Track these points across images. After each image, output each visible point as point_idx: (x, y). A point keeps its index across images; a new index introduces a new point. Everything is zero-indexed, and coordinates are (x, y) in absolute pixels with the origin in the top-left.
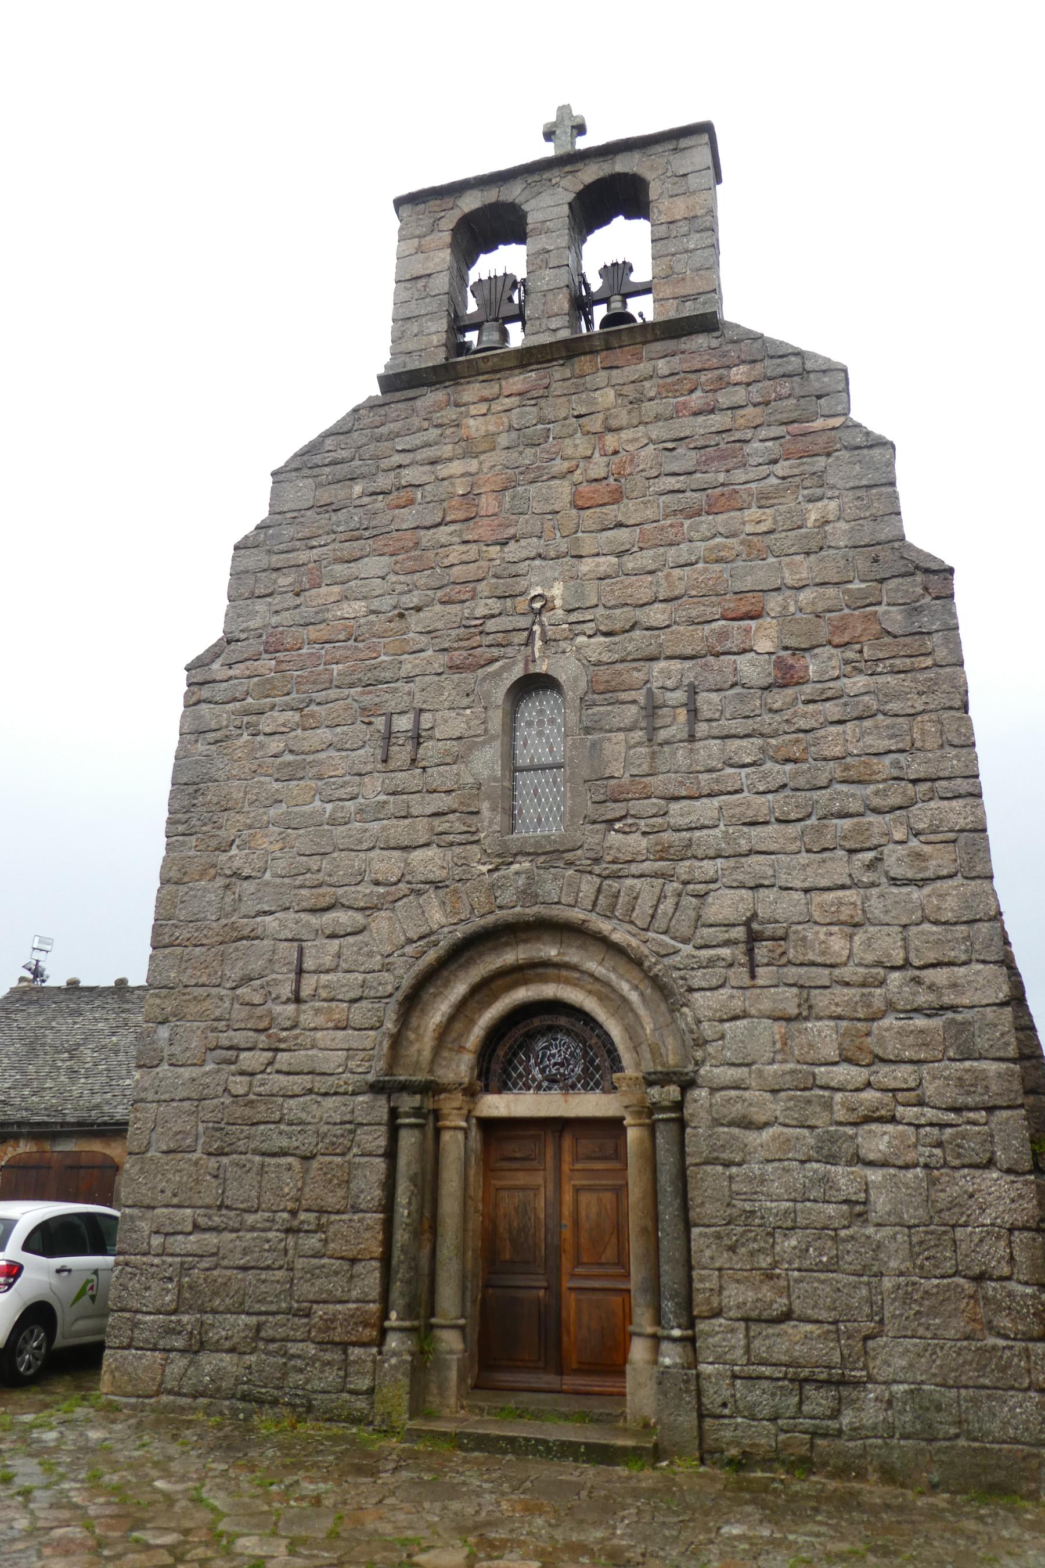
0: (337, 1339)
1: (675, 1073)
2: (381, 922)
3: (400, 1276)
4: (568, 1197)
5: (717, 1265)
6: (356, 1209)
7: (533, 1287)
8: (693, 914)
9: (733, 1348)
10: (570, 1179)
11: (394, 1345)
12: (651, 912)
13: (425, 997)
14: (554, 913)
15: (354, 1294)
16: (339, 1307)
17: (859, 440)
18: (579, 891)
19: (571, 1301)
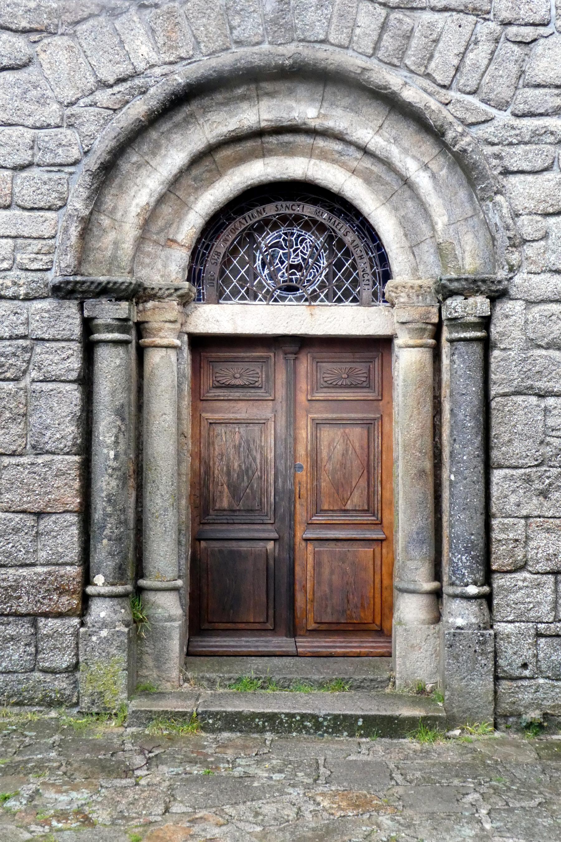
0: (23, 610)
1: (484, 281)
2: (55, 54)
3: (107, 532)
4: (304, 433)
5: (524, 513)
6: (38, 450)
7: (258, 541)
8: (514, 69)
9: (539, 603)
10: (308, 412)
11: (103, 614)
12: (456, 62)
13: (125, 166)
14: (321, 55)
15: (43, 555)
16: (24, 572)
18: (355, 25)
19: (306, 555)
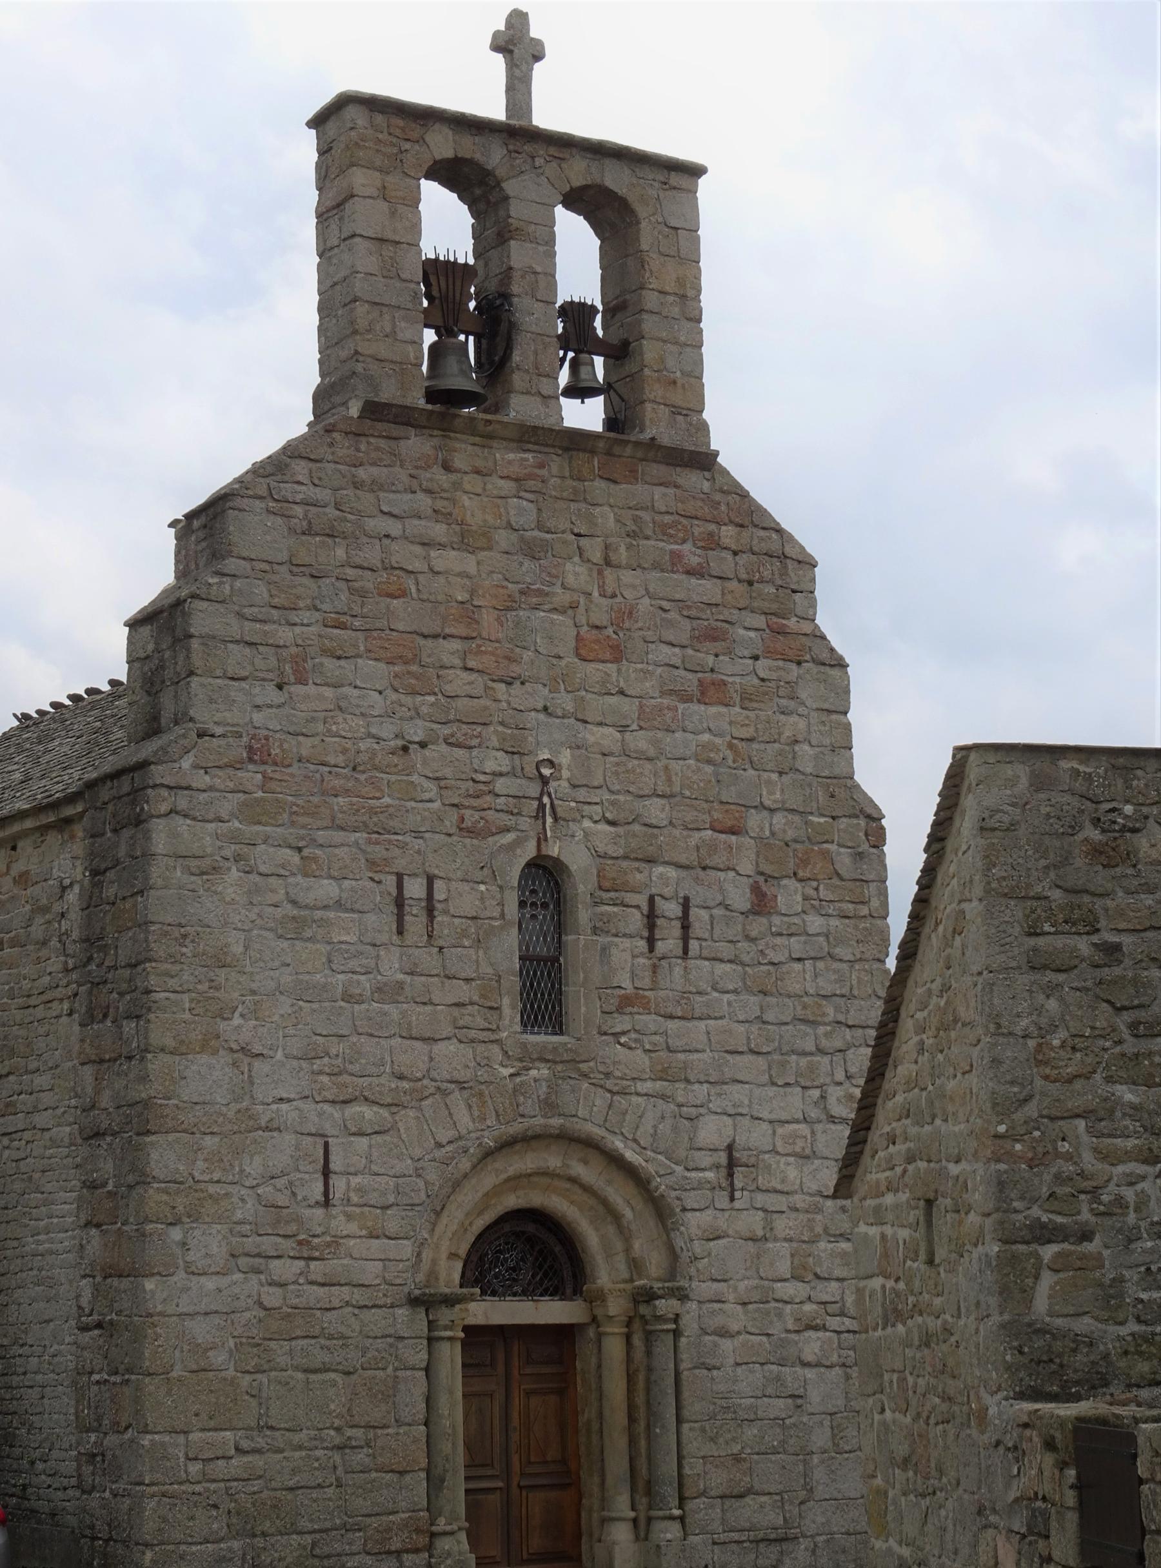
17: (824, 656)
